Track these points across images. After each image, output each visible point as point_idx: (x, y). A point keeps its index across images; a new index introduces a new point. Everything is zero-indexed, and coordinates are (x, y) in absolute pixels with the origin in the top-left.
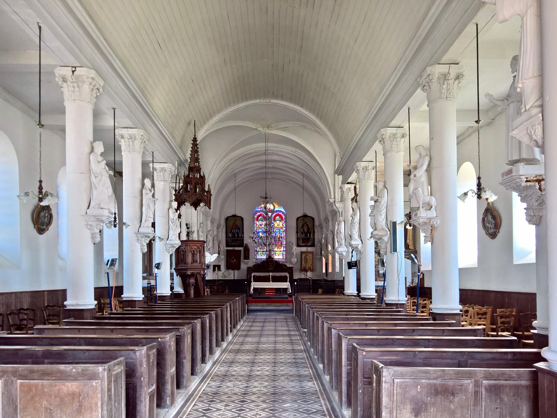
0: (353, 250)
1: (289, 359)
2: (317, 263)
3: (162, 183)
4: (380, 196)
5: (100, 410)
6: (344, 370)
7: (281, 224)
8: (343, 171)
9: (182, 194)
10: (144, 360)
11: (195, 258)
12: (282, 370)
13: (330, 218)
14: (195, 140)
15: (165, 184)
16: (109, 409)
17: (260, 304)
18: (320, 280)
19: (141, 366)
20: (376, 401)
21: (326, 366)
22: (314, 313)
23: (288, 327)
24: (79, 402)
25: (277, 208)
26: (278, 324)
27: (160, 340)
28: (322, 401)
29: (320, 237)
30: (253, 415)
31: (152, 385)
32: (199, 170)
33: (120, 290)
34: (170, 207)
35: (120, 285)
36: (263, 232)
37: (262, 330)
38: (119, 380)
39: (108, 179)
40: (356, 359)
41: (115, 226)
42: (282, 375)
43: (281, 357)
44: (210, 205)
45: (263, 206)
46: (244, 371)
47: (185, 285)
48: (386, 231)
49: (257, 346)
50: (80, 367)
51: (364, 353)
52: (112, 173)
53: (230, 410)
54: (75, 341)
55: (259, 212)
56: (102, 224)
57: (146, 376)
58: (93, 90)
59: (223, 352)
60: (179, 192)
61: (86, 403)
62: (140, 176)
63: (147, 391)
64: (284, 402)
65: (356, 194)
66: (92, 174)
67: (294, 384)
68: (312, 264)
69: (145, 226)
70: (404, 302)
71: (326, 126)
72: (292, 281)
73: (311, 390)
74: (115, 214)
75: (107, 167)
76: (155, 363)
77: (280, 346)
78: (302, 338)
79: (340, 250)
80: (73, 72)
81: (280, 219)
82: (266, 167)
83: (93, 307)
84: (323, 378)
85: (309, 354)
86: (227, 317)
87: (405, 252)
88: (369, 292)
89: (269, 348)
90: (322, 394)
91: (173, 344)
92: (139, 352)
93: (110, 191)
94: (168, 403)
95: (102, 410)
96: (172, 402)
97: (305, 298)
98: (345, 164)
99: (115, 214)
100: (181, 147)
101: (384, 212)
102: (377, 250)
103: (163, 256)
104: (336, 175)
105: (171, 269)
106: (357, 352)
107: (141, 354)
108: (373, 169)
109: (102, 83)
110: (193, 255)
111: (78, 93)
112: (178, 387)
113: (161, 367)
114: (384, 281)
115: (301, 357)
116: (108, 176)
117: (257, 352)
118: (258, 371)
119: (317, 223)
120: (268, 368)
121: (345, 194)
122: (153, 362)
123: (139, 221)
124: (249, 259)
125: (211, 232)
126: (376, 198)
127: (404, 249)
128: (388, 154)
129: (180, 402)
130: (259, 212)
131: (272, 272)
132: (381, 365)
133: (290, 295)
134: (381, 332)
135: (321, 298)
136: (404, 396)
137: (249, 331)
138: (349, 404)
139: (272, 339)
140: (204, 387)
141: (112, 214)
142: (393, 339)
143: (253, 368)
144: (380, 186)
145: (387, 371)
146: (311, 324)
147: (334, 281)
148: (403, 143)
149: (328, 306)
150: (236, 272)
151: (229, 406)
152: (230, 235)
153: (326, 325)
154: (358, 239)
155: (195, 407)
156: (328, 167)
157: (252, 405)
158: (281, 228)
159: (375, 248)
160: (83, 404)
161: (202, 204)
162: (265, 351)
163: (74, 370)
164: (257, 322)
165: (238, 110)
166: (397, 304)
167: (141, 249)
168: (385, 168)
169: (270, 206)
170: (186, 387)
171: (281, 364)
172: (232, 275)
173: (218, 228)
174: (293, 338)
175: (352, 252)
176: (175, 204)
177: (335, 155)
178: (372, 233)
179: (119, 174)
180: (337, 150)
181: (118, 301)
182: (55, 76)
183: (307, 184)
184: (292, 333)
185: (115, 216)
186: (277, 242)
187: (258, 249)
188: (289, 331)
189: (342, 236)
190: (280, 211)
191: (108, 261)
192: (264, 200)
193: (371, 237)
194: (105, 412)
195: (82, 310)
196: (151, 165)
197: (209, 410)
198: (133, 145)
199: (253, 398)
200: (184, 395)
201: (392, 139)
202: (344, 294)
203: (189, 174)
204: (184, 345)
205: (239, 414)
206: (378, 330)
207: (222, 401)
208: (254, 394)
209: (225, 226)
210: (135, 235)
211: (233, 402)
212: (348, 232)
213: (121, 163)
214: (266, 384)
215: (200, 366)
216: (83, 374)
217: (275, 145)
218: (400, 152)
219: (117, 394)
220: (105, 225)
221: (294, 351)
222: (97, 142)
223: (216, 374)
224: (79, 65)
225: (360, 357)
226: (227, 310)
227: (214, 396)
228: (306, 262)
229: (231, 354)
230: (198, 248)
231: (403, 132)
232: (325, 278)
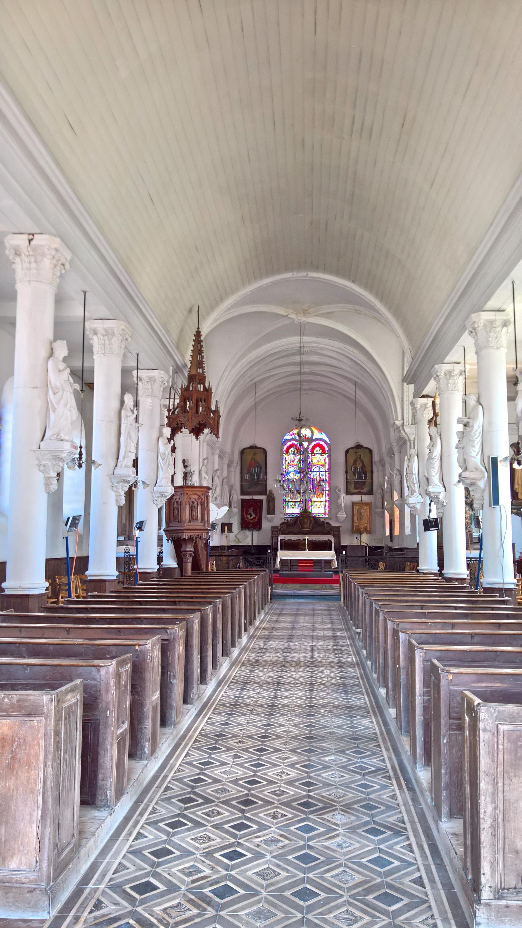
0: (431, 501)
1: (333, 678)
3: (149, 400)
4: (472, 416)
5: (42, 766)
6: (419, 701)
7: (322, 459)
8: (416, 376)
9: (177, 416)
10: (112, 682)
11: (194, 513)
12: (324, 697)
13: (396, 450)
14: (198, 334)
15: (155, 401)
16: (55, 765)
17: (290, 585)
18: (381, 548)
19: (107, 691)
20: (470, 761)
21: (391, 692)
22: (371, 603)
23: (332, 623)
24: (12, 751)
25: (317, 435)
26: (318, 619)
27: (137, 647)
28: (385, 753)
29: (381, 480)
30: (277, 775)
31: (123, 723)
32: (202, 379)
33: (83, 562)
34: (161, 435)
35: (84, 555)
36: (296, 472)
37: (293, 629)
38: (72, 717)
39: (72, 395)
40: (438, 686)
41: (80, 466)
42: (323, 706)
43: (321, 675)
44: (218, 431)
45: (295, 431)
46: (264, 697)
47: (180, 557)
48: (482, 472)
49: (284, 655)
50: (15, 695)
51: (450, 677)
52: (78, 387)
53: (241, 765)
54: (13, 647)
55: (290, 440)
56: (61, 464)
57: (115, 710)
58: (55, 266)
59: (233, 664)
60: (173, 413)
61: (21, 755)
62: (119, 390)
63: (115, 731)
64: (326, 752)
65: (435, 414)
66: (50, 390)
67: (340, 721)
68: (370, 522)
69: (123, 465)
70: (513, 586)
71: (390, 309)
72: (339, 549)
73: (368, 732)
74: (81, 447)
75: (71, 378)
76: (129, 687)
77: (319, 656)
78: (353, 645)
79: (411, 500)
80: (30, 241)
81: (321, 452)
82: (300, 373)
83: (43, 591)
84: (385, 712)
85: (364, 670)
86: (240, 607)
87: (512, 504)
88: (458, 567)
89: (304, 659)
90: (384, 739)
91: (157, 654)
92: (105, 668)
93: (74, 414)
94: (147, 752)
95: (45, 766)
96: (153, 751)
97: (359, 576)
98: (419, 366)
99: (81, 447)
100: (178, 347)
101: (478, 442)
102: (469, 501)
103: (148, 510)
104: (405, 384)
105: (159, 529)
106: (439, 675)
107: (107, 673)
108: (461, 374)
109: (69, 255)
110: (192, 509)
111: (35, 271)
112: (164, 723)
113: (137, 692)
114: (481, 549)
115: (352, 675)
116: (72, 391)
117: (284, 665)
118: (286, 697)
119: (376, 457)
120: (300, 694)
121: (419, 412)
122: (125, 686)
123: (115, 457)
125: (218, 472)
126: (465, 420)
127: (509, 500)
128: (484, 352)
129: (165, 749)
130: (290, 440)
132: (477, 701)
133: (336, 572)
134: (476, 639)
135: (381, 576)
136: (516, 755)
137: (273, 629)
138: (427, 761)
139: (307, 644)
140: (202, 724)
141: (76, 448)
142: (496, 651)
143: (279, 693)
144: (472, 401)
145: (487, 711)
146: (368, 620)
147: (401, 550)
148: (505, 336)
149: (394, 591)
150: (255, 533)
151: (240, 757)
152: (247, 477)
153: (389, 625)
155: (188, 759)
156: (392, 370)
157: (274, 757)
158: (323, 466)
159: (466, 497)
160: (18, 757)
161: (206, 431)
162: (296, 664)
163: (6, 700)
164: (285, 614)
165: (260, 288)
166: (501, 590)
167: (117, 501)
168: (479, 373)
169: (306, 432)
170: (175, 724)
171: (321, 687)
172: (250, 539)
173: (229, 466)
174: (341, 642)
175: (430, 504)
176: (167, 432)
177: (404, 354)
178: (460, 476)
179: (88, 386)
180: (406, 344)
181: (81, 579)
182: (5, 248)
183: (361, 396)
184: (339, 634)
185: (81, 451)
186: (317, 487)
187: (288, 499)
188: (334, 630)
189: (415, 478)
190: (322, 440)
191: (68, 519)
192: (298, 423)
193: (459, 482)
194: (50, 770)
195: (27, 596)
196: (134, 373)
197: (209, 763)
198: (110, 344)
199: (277, 744)
200: (171, 737)
201: (488, 329)
202: (418, 571)
203: (188, 386)
204: (173, 657)
205: (255, 772)
206: (472, 635)
207: (229, 749)
208: (279, 737)
209: (239, 462)
210: (108, 478)
211: (246, 750)
212: (423, 472)
213: (92, 371)
214: (298, 720)
215: (198, 688)
216: (20, 706)
217: (314, 339)
218: (502, 349)
219: (69, 740)
220: (65, 464)
221: (341, 665)
222: (59, 342)
223: (221, 702)
224: (39, 231)
225: (443, 683)
226: (240, 597)
227: (216, 740)
228: (360, 519)
229: (244, 668)
230: (200, 497)
231: (504, 318)
232: (390, 544)
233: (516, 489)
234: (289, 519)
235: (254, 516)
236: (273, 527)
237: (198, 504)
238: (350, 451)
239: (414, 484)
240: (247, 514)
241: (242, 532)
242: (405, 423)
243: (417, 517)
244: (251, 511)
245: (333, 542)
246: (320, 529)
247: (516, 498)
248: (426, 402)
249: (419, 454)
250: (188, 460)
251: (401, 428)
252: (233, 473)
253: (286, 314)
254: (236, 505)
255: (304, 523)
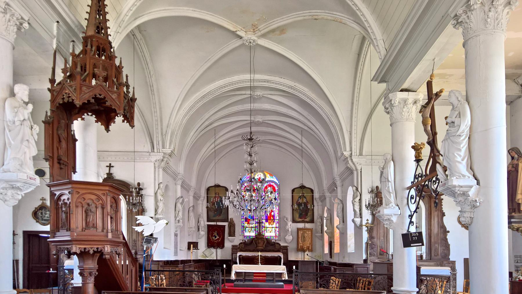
2: (317, 243)
13: (338, 183)
72: (289, 264)
110: (87, 213)
119: (316, 195)
124: (234, 236)
131: (261, 252)
150: (219, 251)
154: (467, 174)
172: (215, 254)
190: (273, 182)
192: (248, 141)
201: (486, 9)
232: (329, 260)
233: (519, 200)
234: (246, 240)
235: (218, 237)
236: (233, 246)
237: (96, 207)
238: (295, 190)
239: (389, 192)
240: (212, 236)
241: (209, 249)
242: (353, 154)
243: (391, 232)
244: (215, 234)
245: (282, 257)
246: (271, 248)
247: (517, 210)
248: (407, 97)
249: (394, 159)
250: (143, 184)
251: (349, 159)
252: (201, 205)
253: (235, 30)
254: (203, 229)
255: (259, 243)
